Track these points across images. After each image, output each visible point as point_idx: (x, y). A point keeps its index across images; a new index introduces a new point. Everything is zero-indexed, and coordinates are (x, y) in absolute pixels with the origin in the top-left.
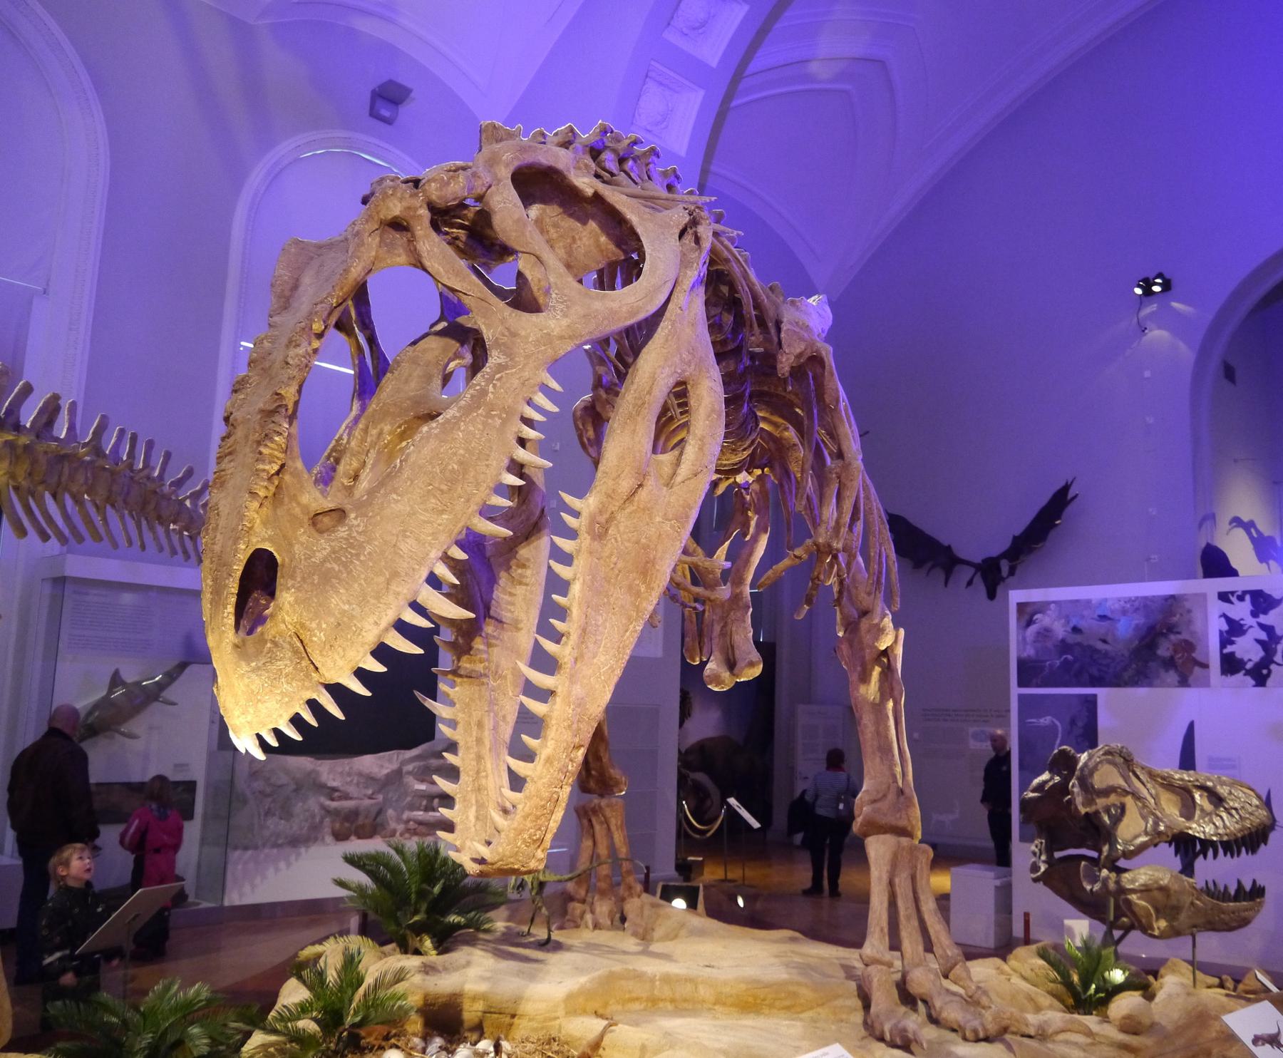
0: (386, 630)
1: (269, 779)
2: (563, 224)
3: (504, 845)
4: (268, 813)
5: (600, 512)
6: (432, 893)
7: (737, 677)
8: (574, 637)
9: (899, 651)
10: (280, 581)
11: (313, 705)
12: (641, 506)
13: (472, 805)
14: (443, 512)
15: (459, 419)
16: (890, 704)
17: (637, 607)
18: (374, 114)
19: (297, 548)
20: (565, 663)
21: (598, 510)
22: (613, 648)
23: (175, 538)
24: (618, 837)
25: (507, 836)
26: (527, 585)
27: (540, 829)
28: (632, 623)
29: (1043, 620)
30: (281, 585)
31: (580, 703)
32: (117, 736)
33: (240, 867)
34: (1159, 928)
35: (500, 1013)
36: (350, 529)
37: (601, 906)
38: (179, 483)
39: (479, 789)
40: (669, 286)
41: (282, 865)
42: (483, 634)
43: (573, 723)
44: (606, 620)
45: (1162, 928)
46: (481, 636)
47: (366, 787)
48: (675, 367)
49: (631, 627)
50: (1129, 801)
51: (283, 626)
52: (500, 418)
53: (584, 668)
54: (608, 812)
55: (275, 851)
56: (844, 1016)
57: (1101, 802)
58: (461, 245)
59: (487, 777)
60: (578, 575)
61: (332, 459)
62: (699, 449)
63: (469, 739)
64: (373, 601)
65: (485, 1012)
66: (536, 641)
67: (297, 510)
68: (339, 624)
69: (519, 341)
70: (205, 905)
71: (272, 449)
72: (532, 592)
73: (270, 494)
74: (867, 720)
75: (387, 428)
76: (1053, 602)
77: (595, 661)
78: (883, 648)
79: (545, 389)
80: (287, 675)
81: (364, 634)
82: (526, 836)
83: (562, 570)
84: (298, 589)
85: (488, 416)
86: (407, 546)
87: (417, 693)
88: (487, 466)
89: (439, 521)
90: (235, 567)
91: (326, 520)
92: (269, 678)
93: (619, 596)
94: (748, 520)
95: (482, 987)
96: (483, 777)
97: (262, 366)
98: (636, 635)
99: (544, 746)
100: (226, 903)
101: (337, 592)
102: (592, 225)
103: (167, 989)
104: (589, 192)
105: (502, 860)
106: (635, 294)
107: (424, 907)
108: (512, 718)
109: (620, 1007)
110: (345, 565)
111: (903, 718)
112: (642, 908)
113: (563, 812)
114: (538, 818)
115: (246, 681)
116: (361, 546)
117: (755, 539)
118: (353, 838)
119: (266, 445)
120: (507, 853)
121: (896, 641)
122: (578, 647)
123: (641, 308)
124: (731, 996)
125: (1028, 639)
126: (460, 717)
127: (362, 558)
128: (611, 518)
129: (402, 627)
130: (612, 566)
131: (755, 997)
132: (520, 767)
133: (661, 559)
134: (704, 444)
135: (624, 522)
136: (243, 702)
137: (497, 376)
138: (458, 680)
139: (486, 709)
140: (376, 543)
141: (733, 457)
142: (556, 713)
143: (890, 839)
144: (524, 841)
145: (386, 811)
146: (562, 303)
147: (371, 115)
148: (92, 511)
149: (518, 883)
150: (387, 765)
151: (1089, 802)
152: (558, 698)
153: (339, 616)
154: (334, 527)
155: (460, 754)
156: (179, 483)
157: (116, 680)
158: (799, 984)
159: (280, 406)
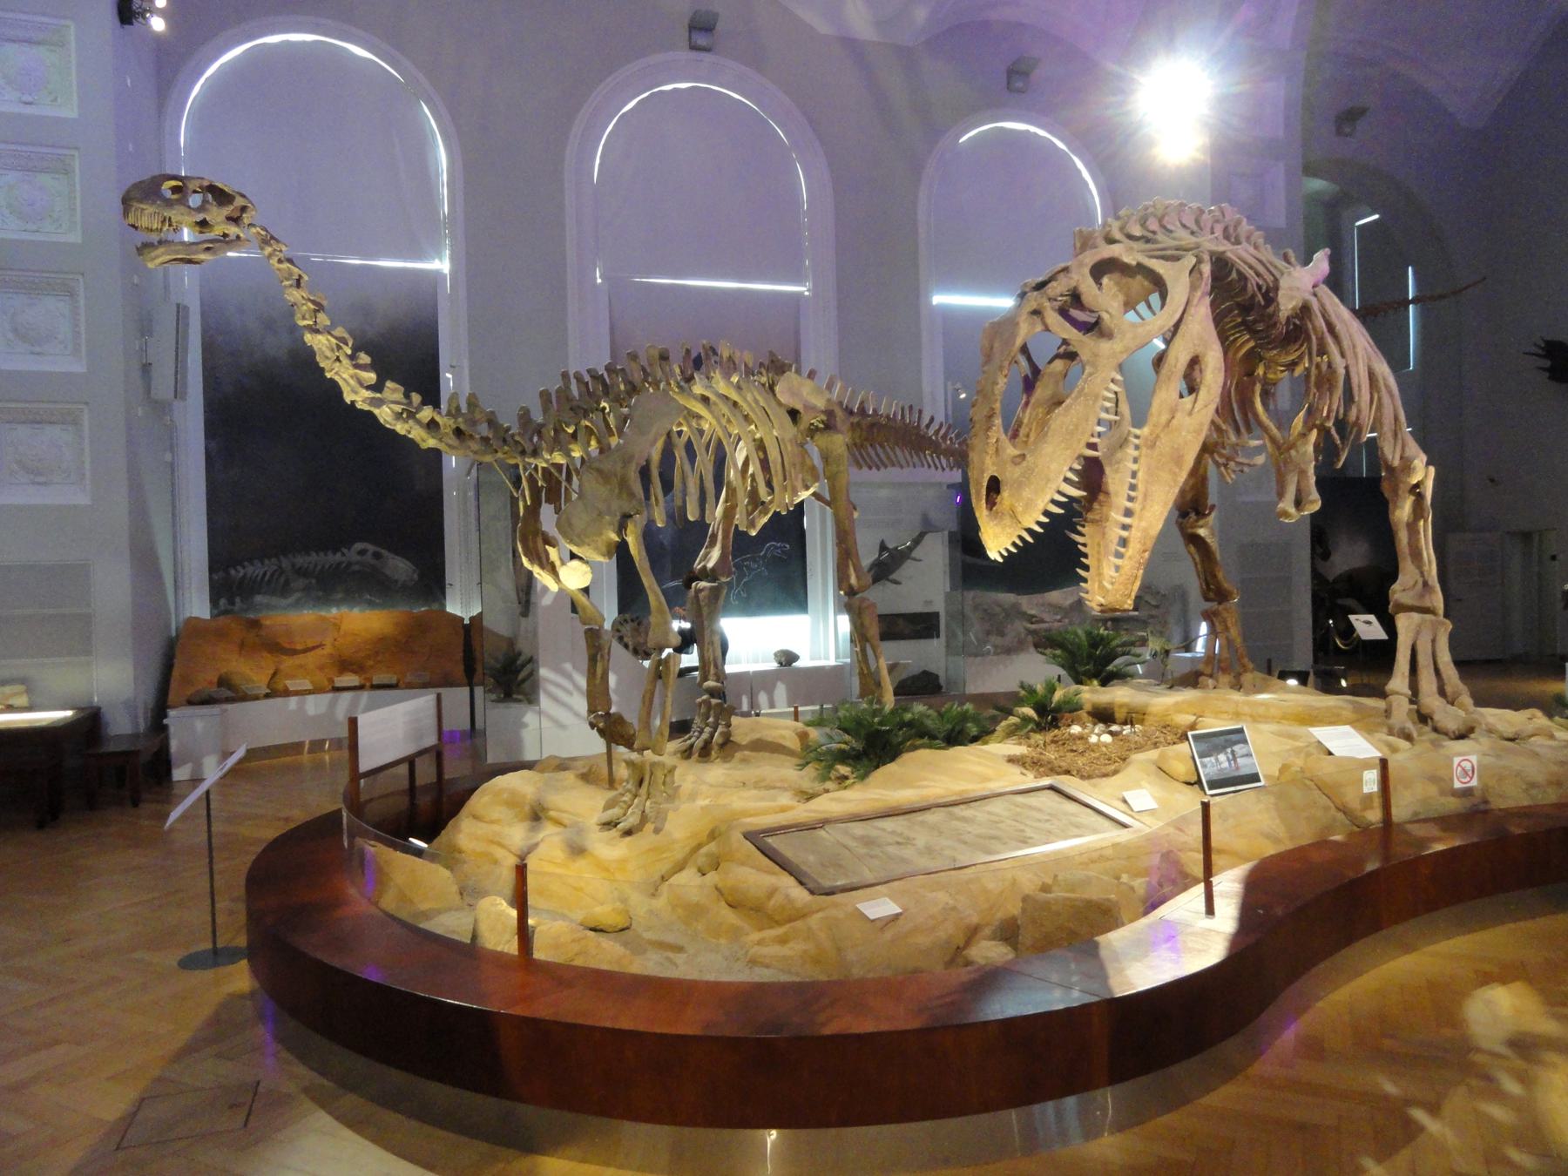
8: (1140, 498)
11: (1020, 537)
31: (1145, 530)
32: (889, 584)
38: (928, 426)
47: (1057, 614)
54: (1225, 615)
75: (1040, 410)
78: (1414, 481)
86: (1054, 466)
87: (1066, 531)
95: (1126, 700)
104: (1134, 263)
121: (1426, 476)
128: (1158, 437)
129: (1054, 502)
142: (1134, 535)
143: (1416, 616)
148: (889, 450)
156: (928, 426)
157: (883, 547)
158: (1341, 708)
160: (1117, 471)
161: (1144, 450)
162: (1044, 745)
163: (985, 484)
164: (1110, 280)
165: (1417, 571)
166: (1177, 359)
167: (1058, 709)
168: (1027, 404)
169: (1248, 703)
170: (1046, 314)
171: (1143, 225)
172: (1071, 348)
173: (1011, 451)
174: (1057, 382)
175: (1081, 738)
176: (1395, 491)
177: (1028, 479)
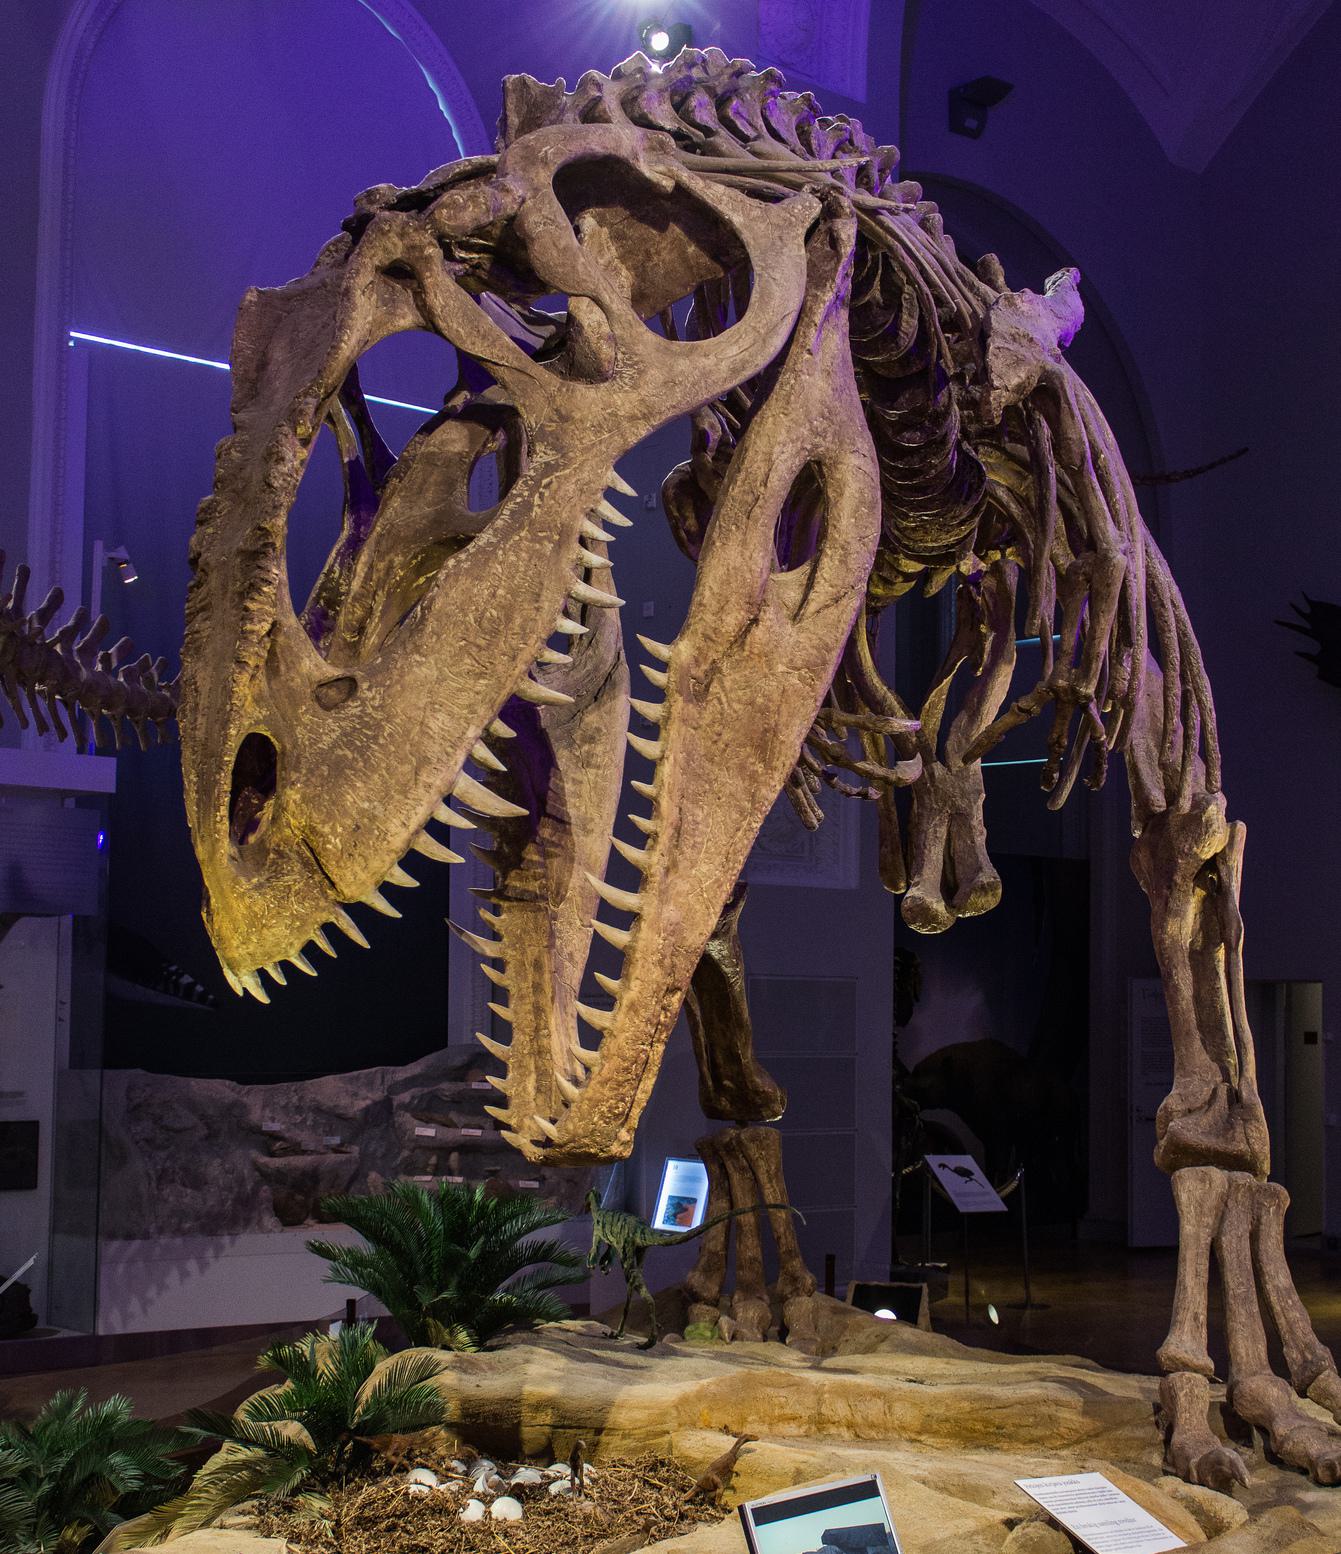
0: (417, 833)
1: (161, 1118)
2: (630, 232)
3: (576, 1120)
4: (163, 1177)
5: (697, 661)
6: (466, 1257)
7: (959, 911)
8: (664, 840)
9: (1237, 861)
10: (280, 773)
11: (329, 929)
12: (756, 651)
13: (530, 1072)
14: (481, 675)
15: (496, 546)
16: (1221, 954)
17: (753, 795)
20: (652, 876)
22: (720, 853)
23: (43, 704)
24: (772, 1193)
25: (579, 1108)
26: (598, 767)
27: (623, 1100)
28: (745, 819)
30: (283, 779)
31: (675, 930)
33: (121, 1269)
35: (579, 1428)
36: (363, 704)
37: (746, 1311)
39: (540, 1053)
40: (789, 322)
41: (192, 1265)
42: (538, 840)
43: (664, 957)
46: (535, 842)
47: (331, 1133)
49: (745, 823)
51: (288, 832)
53: (679, 881)
54: (753, 1151)
55: (178, 1241)
56: (1132, 1454)
58: (484, 276)
59: (549, 1035)
61: (322, 602)
63: (524, 985)
64: (397, 797)
65: (554, 1427)
66: (613, 848)
68: (358, 827)
69: (573, 427)
70: (64, 1334)
71: (261, 603)
72: (604, 778)
74: (1184, 980)
75: (398, 560)
78: (1207, 854)
79: (611, 495)
80: (297, 893)
81: (390, 839)
82: (604, 1109)
83: (648, 748)
86: (438, 723)
88: (537, 609)
89: (478, 688)
90: (226, 759)
92: (275, 897)
93: (732, 783)
94: (982, 638)
95: (552, 1390)
96: (544, 1036)
97: (234, 487)
98: (752, 836)
100: (101, 1332)
101: (353, 787)
102: (675, 230)
103: (69, 1405)
105: (574, 1141)
106: (737, 341)
107: (454, 1282)
108: (582, 956)
110: (361, 751)
111: (1241, 977)
112: (816, 1311)
113: (654, 1080)
114: (620, 1084)
115: (248, 901)
116: (379, 726)
117: (990, 672)
118: (310, 1221)
119: (253, 599)
120: (580, 1131)
122: (670, 853)
123: (747, 362)
124: (947, 1420)
126: (510, 955)
127: (381, 741)
128: (715, 669)
129: (437, 829)
131: (987, 1422)
132: (597, 1017)
133: (787, 726)
135: (730, 677)
136: (243, 928)
137: (545, 482)
138: (505, 905)
139: (546, 943)
140: (398, 721)
141: (944, 536)
142: (646, 943)
143: (1218, 1175)
144: (602, 1116)
145: (367, 1176)
146: (631, 366)
149: (603, 1252)
150: (363, 1092)
152: (643, 924)
153: (357, 817)
155: (512, 1006)
156: (45, 616)
160: (586, 763)
161: (678, 704)
162: (338, 1536)
163: (230, 759)
164: (601, 223)
165: (1215, 1066)
166: (769, 461)
167: (375, 1425)
168: (355, 545)
169: (843, 1392)
171: (680, 107)
172: (493, 395)
173: (313, 665)
174: (449, 485)
175: (442, 1509)
176: (1165, 875)
177: (361, 751)
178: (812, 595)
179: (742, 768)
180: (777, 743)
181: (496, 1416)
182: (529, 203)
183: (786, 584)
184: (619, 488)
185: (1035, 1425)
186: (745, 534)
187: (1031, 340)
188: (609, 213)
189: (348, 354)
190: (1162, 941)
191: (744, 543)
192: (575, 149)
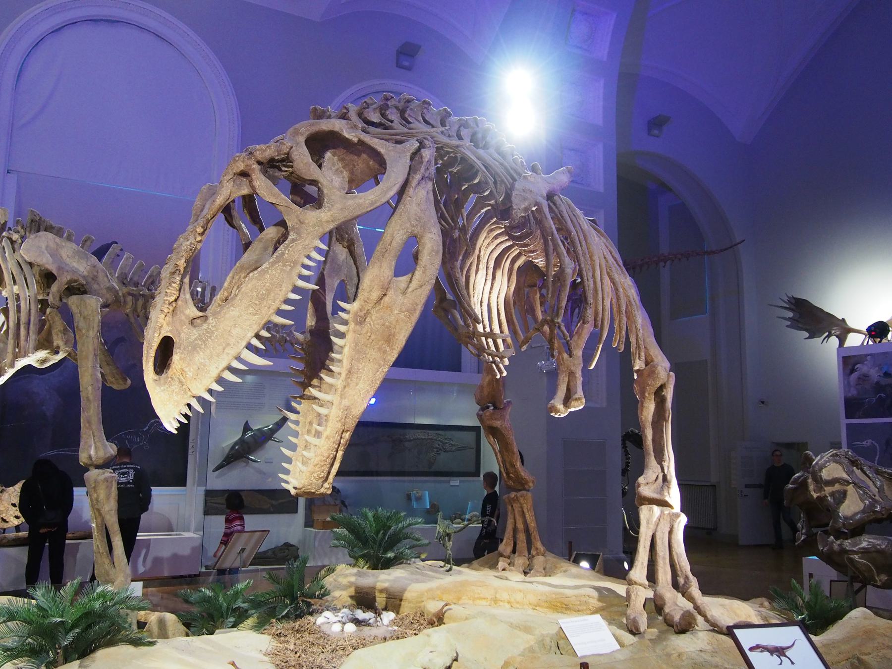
0: (223, 371)
8: (343, 375)
14: (255, 314)
18: (399, 65)
19: (182, 335)
21: (359, 309)
24: (530, 517)
27: (323, 472)
29: (863, 368)
31: (347, 409)
34: (880, 580)
44: (365, 366)
45: (883, 581)
48: (407, 229)
49: (381, 369)
50: (850, 489)
52: (290, 266)
54: (522, 500)
56: (616, 618)
57: (828, 490)
60: (347, 344)
62: (423, 272)
63: (304, 430)
64: (216, 358)
67: (183, 318)
73: (170, 311)
76: (869, 355)
77: (357, 387)
82: (315, 475)
84: (182, 353)
85: (284, 265)
86: (236, 331)
91: (199, 321)
93: (373, 353)
99: (326, 430)
102: (364, 156)
109: (471, 602)
110: (204, 342)
116: (213, 332)
125: (852, 383)
127: (212, 338)
128: (368, 313)
130: (368, 338)
134: (425, 270)
135: (375, 315)
138: (303, 401)
143: (656, 510)
144: (315, 478)
147: (397, 66)
151: (819, 489)
154: (202, 324)
157: (247, 428)
159: (177, 270)
161: (352, 325)
165: (659, 466)
166: (393, 238)
170: (254, 177)
176: (643, 393)
178: (411, 285)
179: (380, 349)
180: (395, 340)
181: (367, 593)
182: (294, 148)
183: (400, 281)
184: (320, 247)
185: (580, 605)
186: (381, 263)
187: (531, 191)
188: (338, 151)
189: (219, 203)
190: (641, 418)
191: (381, 267)
192: (314, 129)
